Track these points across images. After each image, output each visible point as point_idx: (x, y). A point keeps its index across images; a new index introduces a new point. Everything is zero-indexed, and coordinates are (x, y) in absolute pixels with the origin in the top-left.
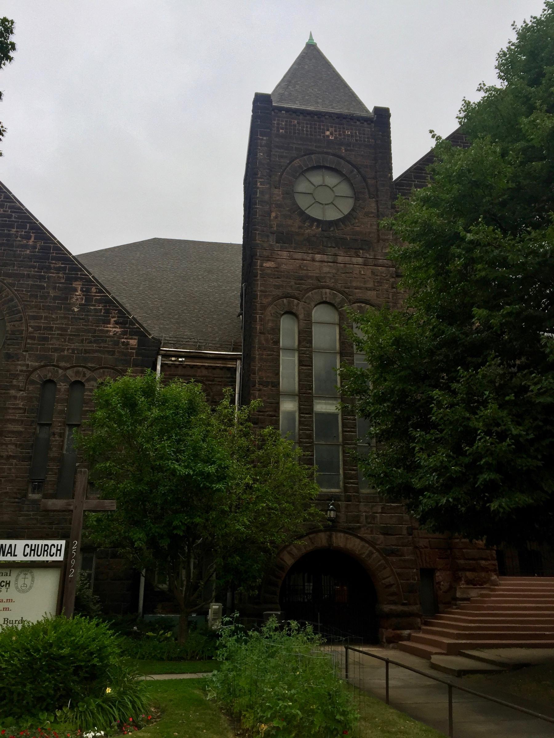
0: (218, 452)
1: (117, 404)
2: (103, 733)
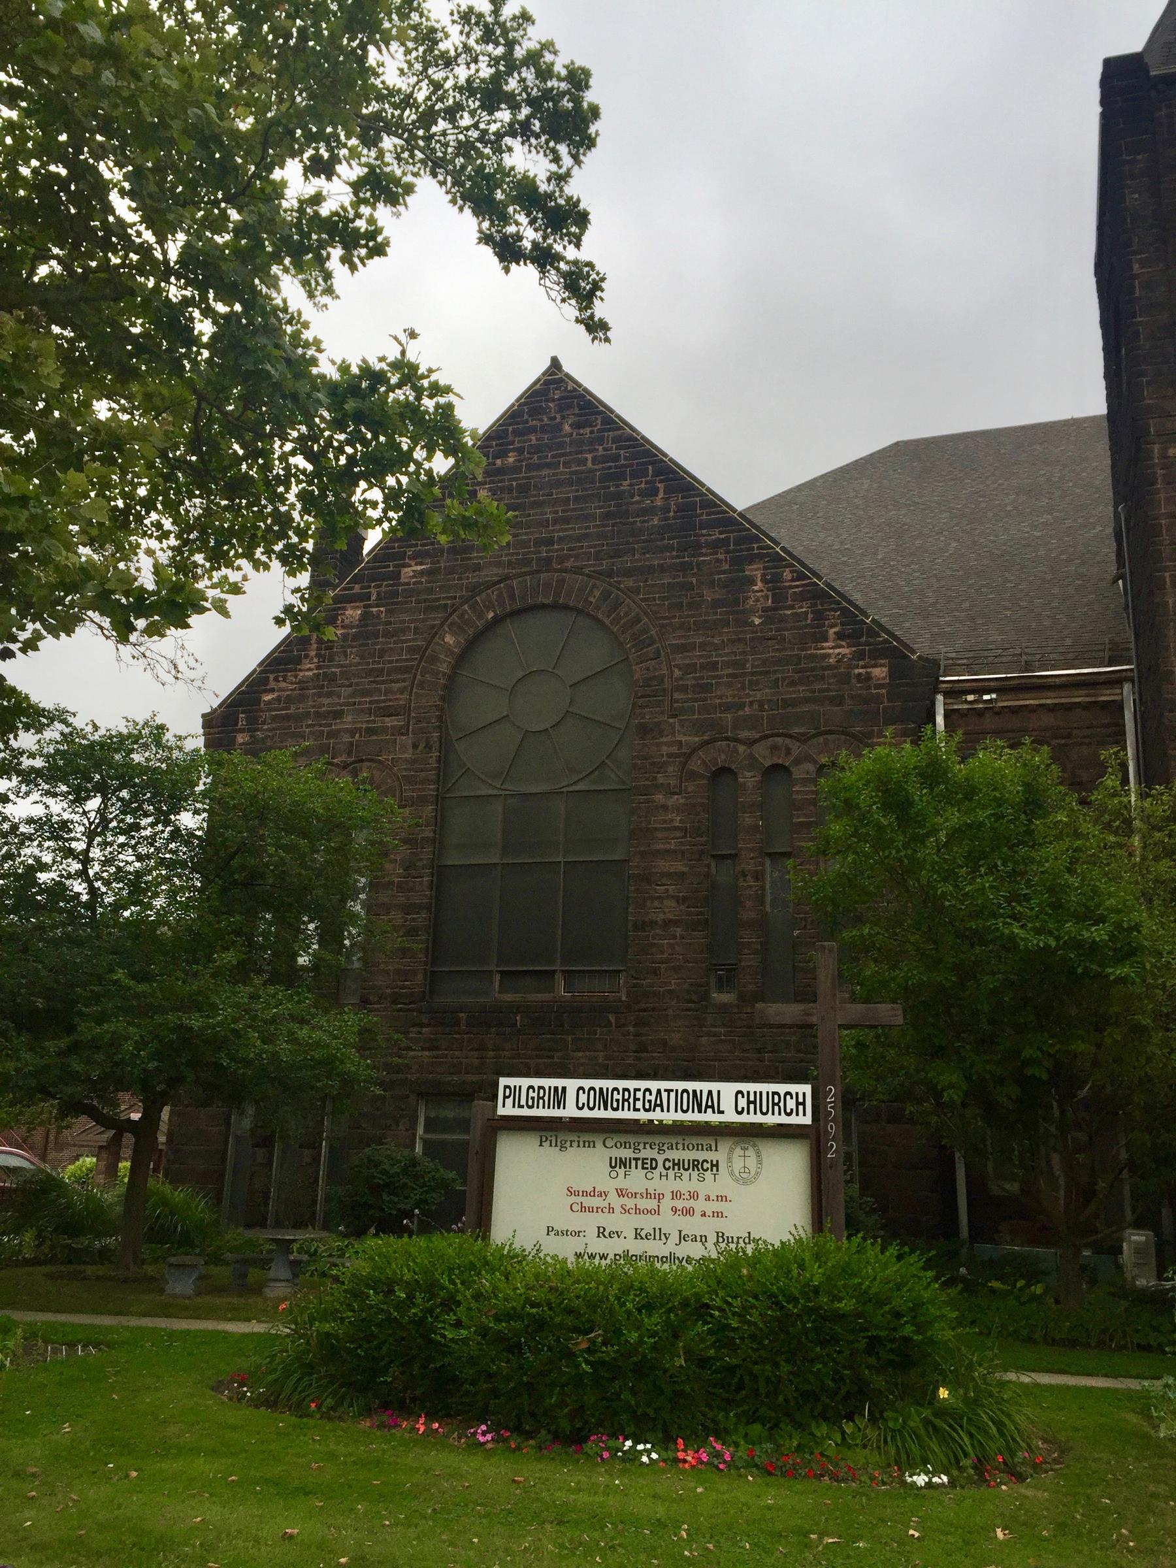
0: (1110, 895)
1: (871, 806)
2: (945, 1478)
